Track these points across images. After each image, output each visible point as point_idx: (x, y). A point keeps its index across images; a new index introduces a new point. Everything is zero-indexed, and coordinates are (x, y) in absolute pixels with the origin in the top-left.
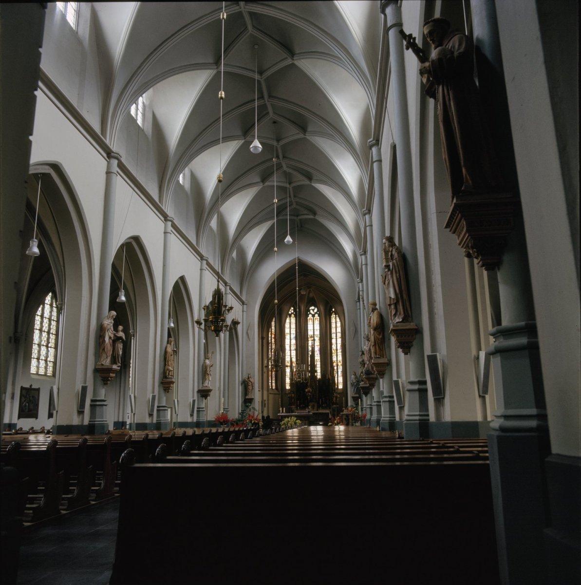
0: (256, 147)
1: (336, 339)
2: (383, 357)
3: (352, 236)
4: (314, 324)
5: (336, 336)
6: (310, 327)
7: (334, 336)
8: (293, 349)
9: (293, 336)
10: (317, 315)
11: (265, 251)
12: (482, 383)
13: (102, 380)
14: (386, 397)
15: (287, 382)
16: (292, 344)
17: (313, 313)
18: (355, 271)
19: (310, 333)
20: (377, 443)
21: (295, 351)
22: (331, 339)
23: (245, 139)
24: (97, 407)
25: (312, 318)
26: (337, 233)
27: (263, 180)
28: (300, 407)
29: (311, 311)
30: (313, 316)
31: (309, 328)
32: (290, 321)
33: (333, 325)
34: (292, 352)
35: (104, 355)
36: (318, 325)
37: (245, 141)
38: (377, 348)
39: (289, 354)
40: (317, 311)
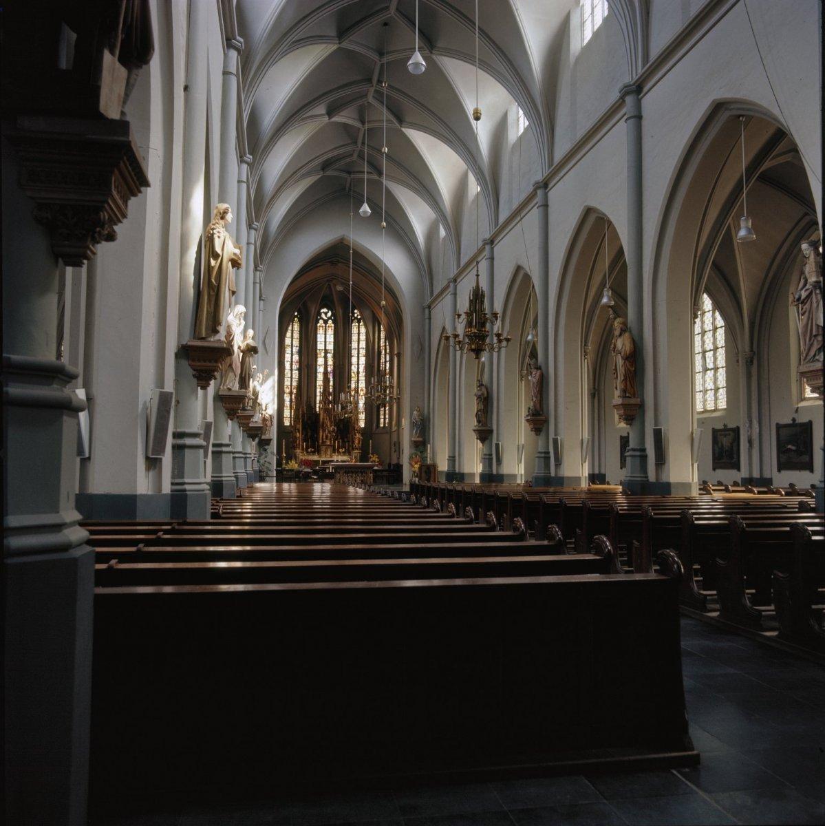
0: (417, 64)
1: (358, 357)
2: (634, 397)
3: (446, 218)
4: (325, 334)
5: (358, 354)
6: (320, 338)
7: (354, 352)
8: (295, 368)
9: (295, 350)
10: (330, 322)
11: (298, 219)
12: (172, 410)
13: (226, 413)
14: (634, 450)
15: (285, 416)
16: (294, 360)
17: (325, 318)
18: (424, 265)
19: (320, 346)
20: (765, 522)
21: (297, 372)
22: (350, 356)
23: (340, 43)
24: (186, 450)
25: (324, 325)
26: (407, 207)
27: (331, 112)
28: (307, 452)
29: (323, 316)
30: (326, 322)
31: (319, 340)
32: (359, 330)
33: (355, 338)
34: (294, 372)
35: (231, 374)
36: (332, 336)
37: (339, 49)
38: (628, 383)
39: (289, 375)
40: (332, 316)
